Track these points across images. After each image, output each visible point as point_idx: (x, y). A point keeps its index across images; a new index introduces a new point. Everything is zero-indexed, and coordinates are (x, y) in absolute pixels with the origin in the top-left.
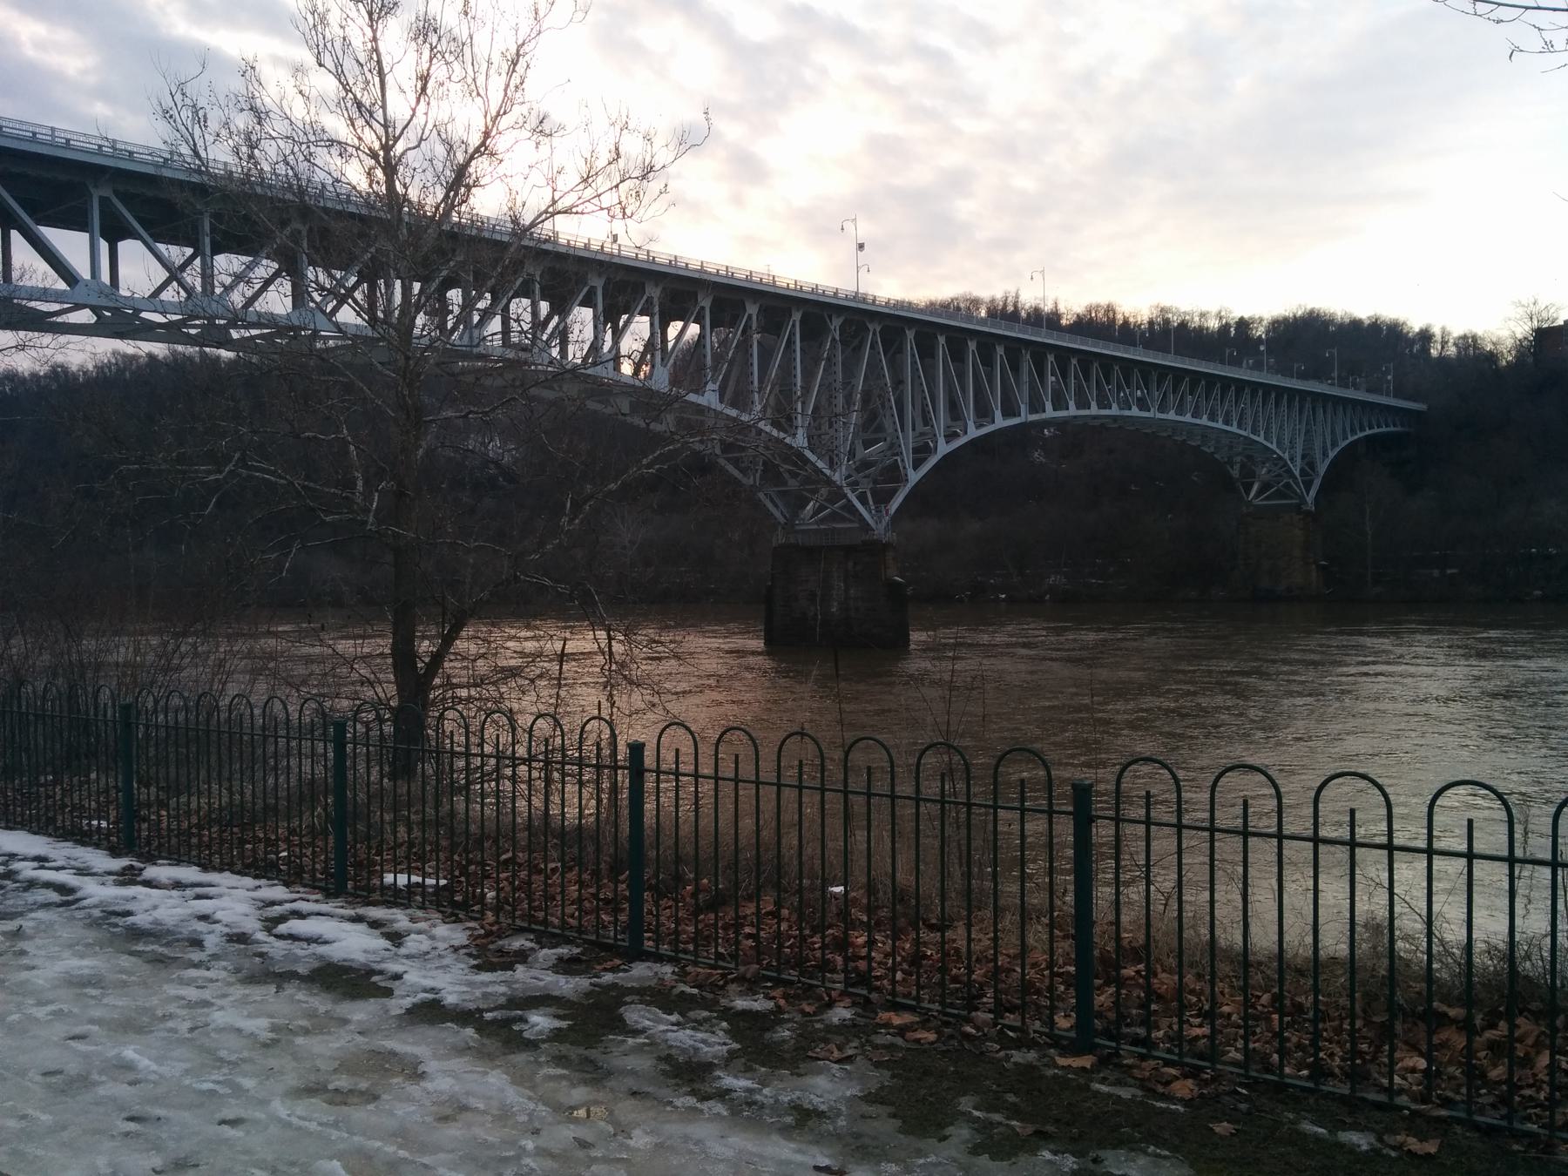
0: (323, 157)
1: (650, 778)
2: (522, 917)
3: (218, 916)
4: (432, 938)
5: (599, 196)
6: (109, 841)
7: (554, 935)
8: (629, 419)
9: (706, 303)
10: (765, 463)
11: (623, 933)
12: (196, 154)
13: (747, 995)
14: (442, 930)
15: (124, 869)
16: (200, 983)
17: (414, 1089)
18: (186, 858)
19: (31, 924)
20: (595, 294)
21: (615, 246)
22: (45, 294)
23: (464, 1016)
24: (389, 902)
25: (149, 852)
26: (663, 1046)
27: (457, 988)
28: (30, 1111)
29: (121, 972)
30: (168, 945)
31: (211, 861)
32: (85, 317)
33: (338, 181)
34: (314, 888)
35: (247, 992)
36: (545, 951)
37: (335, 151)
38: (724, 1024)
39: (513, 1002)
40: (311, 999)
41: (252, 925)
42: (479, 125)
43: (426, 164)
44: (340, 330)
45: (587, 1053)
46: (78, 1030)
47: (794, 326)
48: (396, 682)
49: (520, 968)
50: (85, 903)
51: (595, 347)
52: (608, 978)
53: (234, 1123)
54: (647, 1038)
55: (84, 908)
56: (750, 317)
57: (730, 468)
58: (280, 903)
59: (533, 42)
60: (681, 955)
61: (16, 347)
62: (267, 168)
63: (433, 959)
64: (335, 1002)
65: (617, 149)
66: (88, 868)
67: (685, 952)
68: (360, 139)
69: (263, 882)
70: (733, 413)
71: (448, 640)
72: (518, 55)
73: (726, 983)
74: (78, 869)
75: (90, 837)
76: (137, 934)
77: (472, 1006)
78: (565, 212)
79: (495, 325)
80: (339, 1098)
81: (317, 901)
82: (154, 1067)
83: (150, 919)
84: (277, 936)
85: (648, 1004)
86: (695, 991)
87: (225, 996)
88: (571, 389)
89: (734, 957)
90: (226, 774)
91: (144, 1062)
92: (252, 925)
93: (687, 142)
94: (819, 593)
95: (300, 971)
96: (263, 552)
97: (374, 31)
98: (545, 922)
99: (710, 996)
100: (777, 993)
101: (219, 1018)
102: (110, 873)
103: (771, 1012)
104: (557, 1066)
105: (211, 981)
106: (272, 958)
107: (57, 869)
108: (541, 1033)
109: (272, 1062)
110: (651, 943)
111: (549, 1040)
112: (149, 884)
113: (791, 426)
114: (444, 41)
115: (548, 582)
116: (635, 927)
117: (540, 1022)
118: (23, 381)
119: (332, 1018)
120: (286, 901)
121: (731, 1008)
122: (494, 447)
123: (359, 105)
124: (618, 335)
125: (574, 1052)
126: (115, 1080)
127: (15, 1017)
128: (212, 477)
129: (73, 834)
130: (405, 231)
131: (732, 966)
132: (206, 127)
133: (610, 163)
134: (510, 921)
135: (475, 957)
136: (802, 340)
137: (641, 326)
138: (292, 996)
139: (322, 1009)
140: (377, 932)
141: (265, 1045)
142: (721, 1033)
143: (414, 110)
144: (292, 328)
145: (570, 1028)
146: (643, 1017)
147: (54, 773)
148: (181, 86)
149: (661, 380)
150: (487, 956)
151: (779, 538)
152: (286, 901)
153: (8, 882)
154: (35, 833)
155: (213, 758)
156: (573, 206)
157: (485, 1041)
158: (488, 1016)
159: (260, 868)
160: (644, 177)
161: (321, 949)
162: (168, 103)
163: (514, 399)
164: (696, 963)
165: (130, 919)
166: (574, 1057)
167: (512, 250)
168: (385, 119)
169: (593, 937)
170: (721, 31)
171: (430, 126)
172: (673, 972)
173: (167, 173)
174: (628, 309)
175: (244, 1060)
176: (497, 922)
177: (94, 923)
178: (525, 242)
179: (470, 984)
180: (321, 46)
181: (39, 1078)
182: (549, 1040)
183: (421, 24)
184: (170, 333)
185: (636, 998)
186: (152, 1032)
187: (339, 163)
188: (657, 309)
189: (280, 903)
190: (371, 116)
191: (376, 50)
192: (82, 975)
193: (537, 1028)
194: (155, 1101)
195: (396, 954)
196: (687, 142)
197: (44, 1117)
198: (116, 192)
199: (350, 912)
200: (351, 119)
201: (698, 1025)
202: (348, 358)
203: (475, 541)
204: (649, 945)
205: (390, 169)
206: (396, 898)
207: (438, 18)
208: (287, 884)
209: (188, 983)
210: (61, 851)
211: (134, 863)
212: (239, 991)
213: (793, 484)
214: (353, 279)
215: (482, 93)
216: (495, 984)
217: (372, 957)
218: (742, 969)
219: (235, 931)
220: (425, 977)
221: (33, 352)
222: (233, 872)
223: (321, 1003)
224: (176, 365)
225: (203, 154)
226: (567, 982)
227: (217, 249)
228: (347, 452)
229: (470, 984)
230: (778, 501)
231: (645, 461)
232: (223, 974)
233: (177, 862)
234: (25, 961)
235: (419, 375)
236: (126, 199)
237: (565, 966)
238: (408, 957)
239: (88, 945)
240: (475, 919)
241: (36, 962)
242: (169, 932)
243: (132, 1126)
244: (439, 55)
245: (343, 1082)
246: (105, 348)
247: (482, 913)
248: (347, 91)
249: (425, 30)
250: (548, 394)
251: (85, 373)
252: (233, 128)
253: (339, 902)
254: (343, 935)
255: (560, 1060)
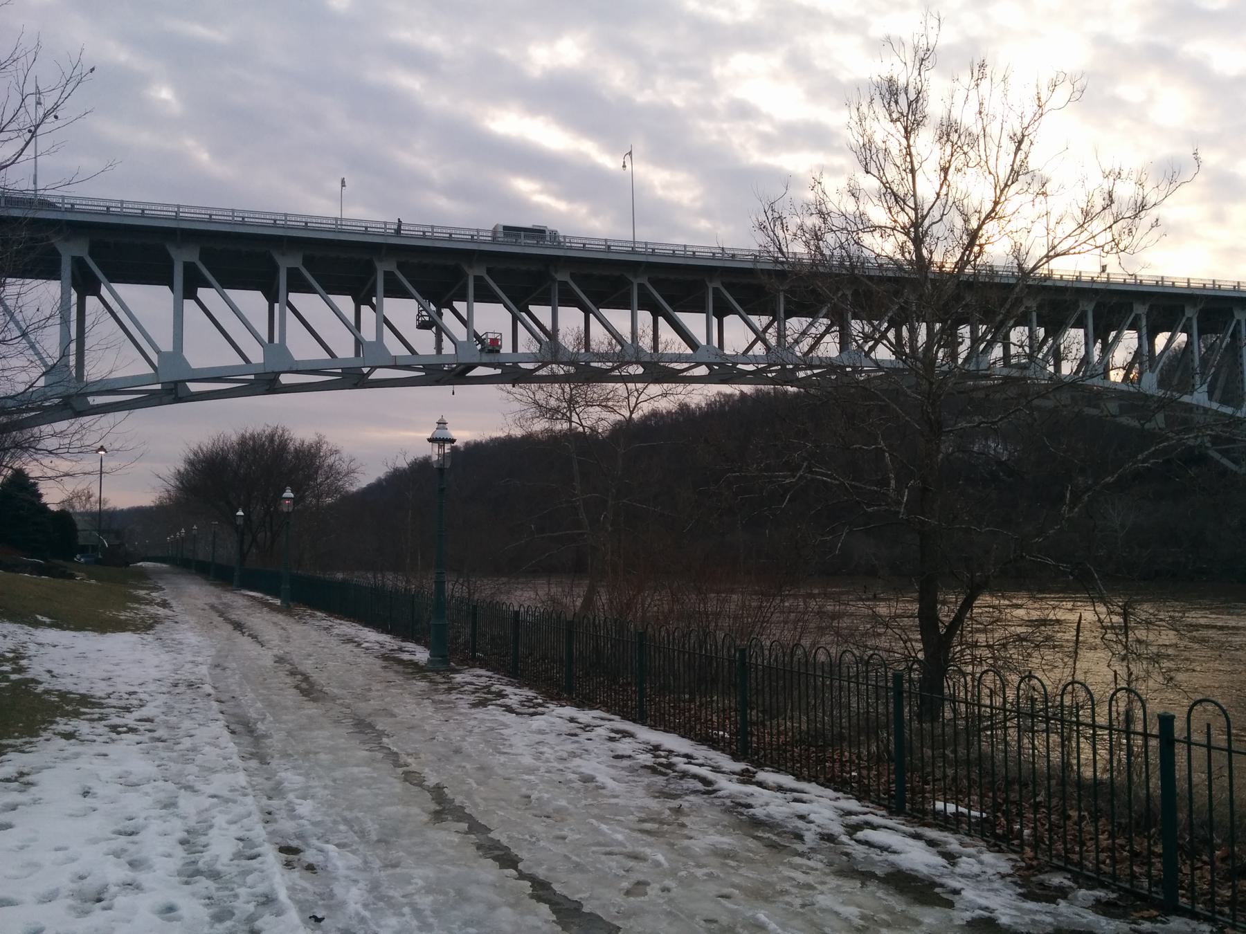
0: (867, 239)
1: (1180, 751)
2: (1058, 856)
3: (812, 817)
4: (981, 862)
5: (1094, 237)
6: (731, 748)
7: (1089, 878)
9: (1191, 312)
12: (780, 250)
14: (988, 857)
15: (743, 771)
21: (1104, 275)
22: (679, 358)
24: (941, 826)
25: (758, 759)
27: (1008, 911)
29: (749, 851)
30: (778, 834)
31: (801, 773)
32: (702, 371)
33: (879, 255)
34: (880, 805)
35: (840, 883)
36: (1083, 892)
37: (877, 234)
40: (890, 898)
41: (837, 829)
42: (990, 196)
43: (946, 234)
46: (726, 891)
48: (922, 640)
49: (1063, 904)
50: (720, 794)
51: (1085, 361)
55: (719, 797)
57: (1225, 461)
58: (856, 814)
59: (1037, 123)
60: (1218, 916)
61: (661, 395)
63: (984, 881)
64: (908, 904)
65: (1110, 196)
66: (719, 767)
68: (895, 221)
69: (840, 795)
70: (1228, 410)
71: (968, 604)
72: (1023, 136)
74: (713, 767)
75: (718, 743)
76: (756, 823)
78: (1064, 254)
79: (998, 352)
81: (883, 816)
87: (823, 883)
88: (1065, 398)
90: (804, 706)
92: (837, 829)
93: (1172, 175)
95: (878, 872)
101: (823, 900)
102: (734, 773)
105: (812, 869)
106: (855, 859)
107: (701, 765)
110: (1184, 900)
112: (760, 784)
114: (963, 137)
115: (1050, 562)
116: (1170, 882)
118: (662, 416)
119: (906, 917)
120: (860, 813)
122: (994, 447)
124: (1107, 349)
127: (683, 873)
128: (788, 481)
130: (930, 286)
132: (787, 230)
133: (1104, 209)
134: (1046, 858)
135: (1021, 886)
137: (1129, 341)
138: (873, 893)
139: (899, 908)
140: (934, 850)
148: (771, 205)
149: (1150, 383)
152: (860, 813)
154: (683, 737)
155: (796, 693)
156: (1070, 249)
160: (1136, 216)
161: (892, 857)
162: (762, 218)
163: (1020, 409)
165: (752, 811)
167: (1017, 289)
168: (916, 204)
169: (1127, 886)
171: (950, 203)
173: (759, 266)
176: (1035, 858)
177: (727, 811)
179: (1018, 909)
180: (869, 158)
181: (702, 923)
183: (944, 128)
184: (756, 377)
186: (774, 902)
187: (880, 243)
188: (1144, 323)
189: (856, 814)
190: (905, 203)
191: (910, 154)
192: (722, 849)
195: (952, 872)
196: (1172, 175)
199: (911, 830)
200: (889, 208)
202: (885, 386)
203: (987, 526)
204: (1183, 901)
205: (918, 242)
207: (959, 121)
208: (859, 799)
209: (796, 867)
210: (701, 752)
211: (749, 768)
212: (833, 882)
214: (886, 325)
215: (993, 171)
217: (933, 871)
219: (826, 831)
220: (980, 896)
221: (671, 398)
222: (818, 783)
223: (897, 903)
224: (758, 398)
225: (785, 250)
226: (1108, 924)
227: (789, 315)
229: (1018, 909)
231: (1140, 457)
232: (820, 866)
233: (778, 771)
235: (940, 396)
236: (729, 287)
238: (963, 876)
241: (692, 834)
242: (779, 825)
246: (713, 390)
248: (886, 188)
249: (948, 131)
250: (1049, 403)
254: (908, 849)
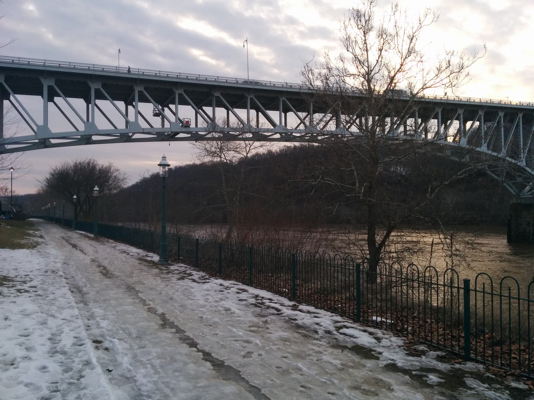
1: (472, 294)
2: (422, 338)
3: (322, 324)
4: (391, 341)
6: (288, 296)
7: (435, 347)
8: (451, 158)
10: (507, 172)
11: (461, 349)
12: (311, 84)
13: (516, 381)
14: (394, 339)
15: (293, 305)
16: (318, 345)
17: (390, 394)
18: (310, 304)
19: (269, 319)
20: (438, 114)
21: (446, 97)
22: (268, 130)
23: (405, 371)
24: (375, 326)
26: (482, 396)
27: (401, 361)
28: (273, 378)
30: (308, 331)
32: (278, 136)
35: (333, 351)
36: (432, 352)
38: (508, 392)
39: (422, 369)
40: (353, 356)
41: (332, 328)
42: (399, 62)
44: (352, 134)
45: (453, 393)
46: (285, 355)
47: (519, 119)
50: (283, 315)
51: (437, 133)
52: (457, 366)
53: (333, 394)
54: (475, 391)
56: (500, 117)
57: (493, 175)
58: (340, 322)
59: (419, 31)
60: (486, 362)
62: (331, 85)
64: (361, 359)
67: (488, 360)
69: (334, 314)
70: (495, 154)
71: (387, 236)
72: (413, 36)
73: (506, 375)
76: (299, 327)
77: (407, 368)
78: (430, 87)
79: (402, 129)
80: (365, 393)
81: (351, 323)
82: (307, 371)
83: (302, 322)
84: (340, 333)
85: (475, 378)
86: (494, 377)
87: (326, 351)
89: (508, 365)
91: (304, 369)
92: (332, 328)
94: (531, 222)
96: (328, 206)
97: (365, 37)
98: (431, 341)
99: (500, 379)
100: (529, 382)
101: (325, 358)
102: (290, 306)
103: (527, 390)
104: (441, 396)
105: (321, 345)
106: (339, 341)
107: (276, 303)
108: (434, 382)
109: (343, 376)
110: (473, 355)
111: (436, 385)
112: (300, 311)
113: (518, 157)
114: (388, 36)
115: (422, 217)
116: (467, 348)
117: (433, 378)
118: (260, 155)
119: (360, 364)
121: (510, 386)
123: (360, 61)
124: (447, 128)
125: (448, 392)
126: (296, 373)
128: (314, 183)
129: (278, 293)
130: (374, 100)
131: (509, 369)
133: (446, 68)
135: (407, 351)
136: (523, 124)
140: (372, 336)
141: (340, 370)
142: (506, 395)
143: (378, 61)
144: (336, 135)
145: (445, 382)
146: (474, 383)
147: (271, 273)
148: (307, 64)
149: (464, 143)
150: (412, 352)
151: (514, 201)
153: (262, 306)
154: (268, 291)
156: (432, 85)
157: (414, 382)
158: (414, 373)
159: (332, 310)
160: (459, 72)
161: (354, 340)
162: (303, 70)
164: (493, 366)
165: (297, 322)
166: (447, 394)
167: (410, 102)
168: (368, 65)
169: (450, 350)
170: (485, 9)
171: (382, 65)
172: (483, 368)
173: (302, 91)
174: (452, 119)
175: (334, 374)
176: (413, 339)
177: (286, 322)
178: (415, 99)
182: (436, 385)
183: (380, 32)
184: (301, 139)
185: (470, 375)
189: (340, 322)
191: (366, 43)
192: (284, 338)
193: (432, 381)
194: (309, 382)
195: (379, 345)
197: (278, 381)
198: (287, 99)
200: (357, 67)
201: (496, 390)
202: (354, 143)
203: (396, 202)
204: (472, 356)
205: (369, 81)
206: (377, 325)
207: (386, 29)
208: (341, 316)
209: (315, 345)
210: (276, 298)
212: (330, 350)
213: (519, 180)
214: (355, 117)
216: (414, 362)
217: (371, 345)
218: (513, 371)
220: (390, 355)
221: (264, 147)
222: (324, 310)
223: (356, 358)
224: (302, 148)
225: (313, 84)
226: (442, 365)
227: (315, 112)
228: (354, 174)
229: (405, 360)
230: (513, 186)
231: (459, 173)
232: (325, 344)
233: (308, 305)
234: (269, 331)
236: (290, 100)
237: (439, 359)
238: (383, 347)
239: (285, 328)
240: (405, 337)
241: (271, 332)
242: (308, 327)
243: (302, 389)
244: (386, 42)
245: (365, 387)
246: (282, 145)
247: (407, 334)
251: (277, 152)
252: (321, 75)
253: (358, 324)
254: (361, 336)
255: (442, 394)
